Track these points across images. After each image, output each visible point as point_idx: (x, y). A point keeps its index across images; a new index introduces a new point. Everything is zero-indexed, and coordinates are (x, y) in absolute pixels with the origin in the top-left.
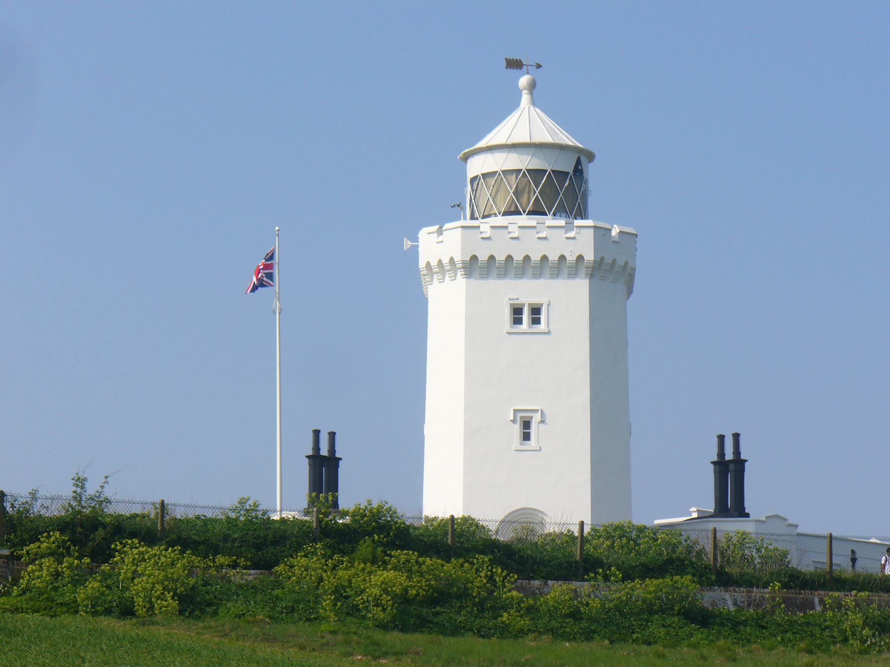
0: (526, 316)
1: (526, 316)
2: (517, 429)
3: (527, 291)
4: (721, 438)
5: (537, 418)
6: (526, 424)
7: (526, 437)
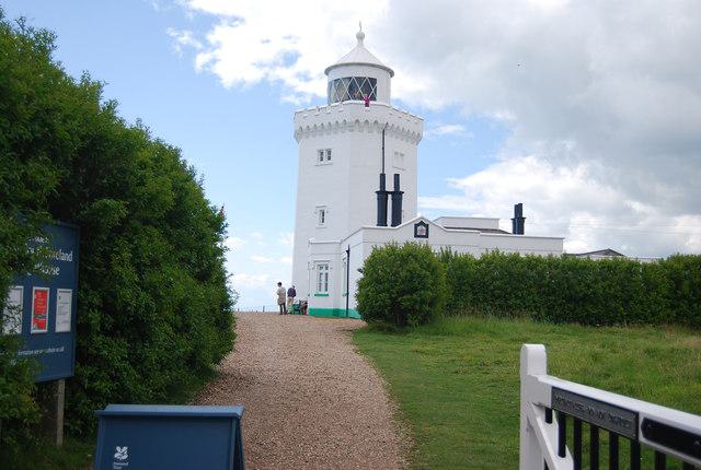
0: (325, 155)
1: (325, 155)
2: (318, 217)
3: (324, 142)
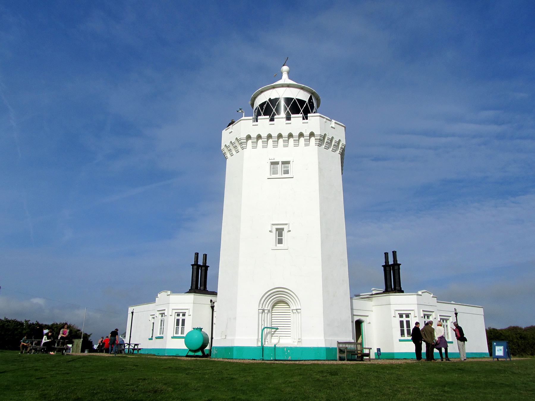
2: (273, 236)
3: (280, 153)
4: (386, 254)
5: (286, 228)
6: (280, 232)
7: (280, 241)
